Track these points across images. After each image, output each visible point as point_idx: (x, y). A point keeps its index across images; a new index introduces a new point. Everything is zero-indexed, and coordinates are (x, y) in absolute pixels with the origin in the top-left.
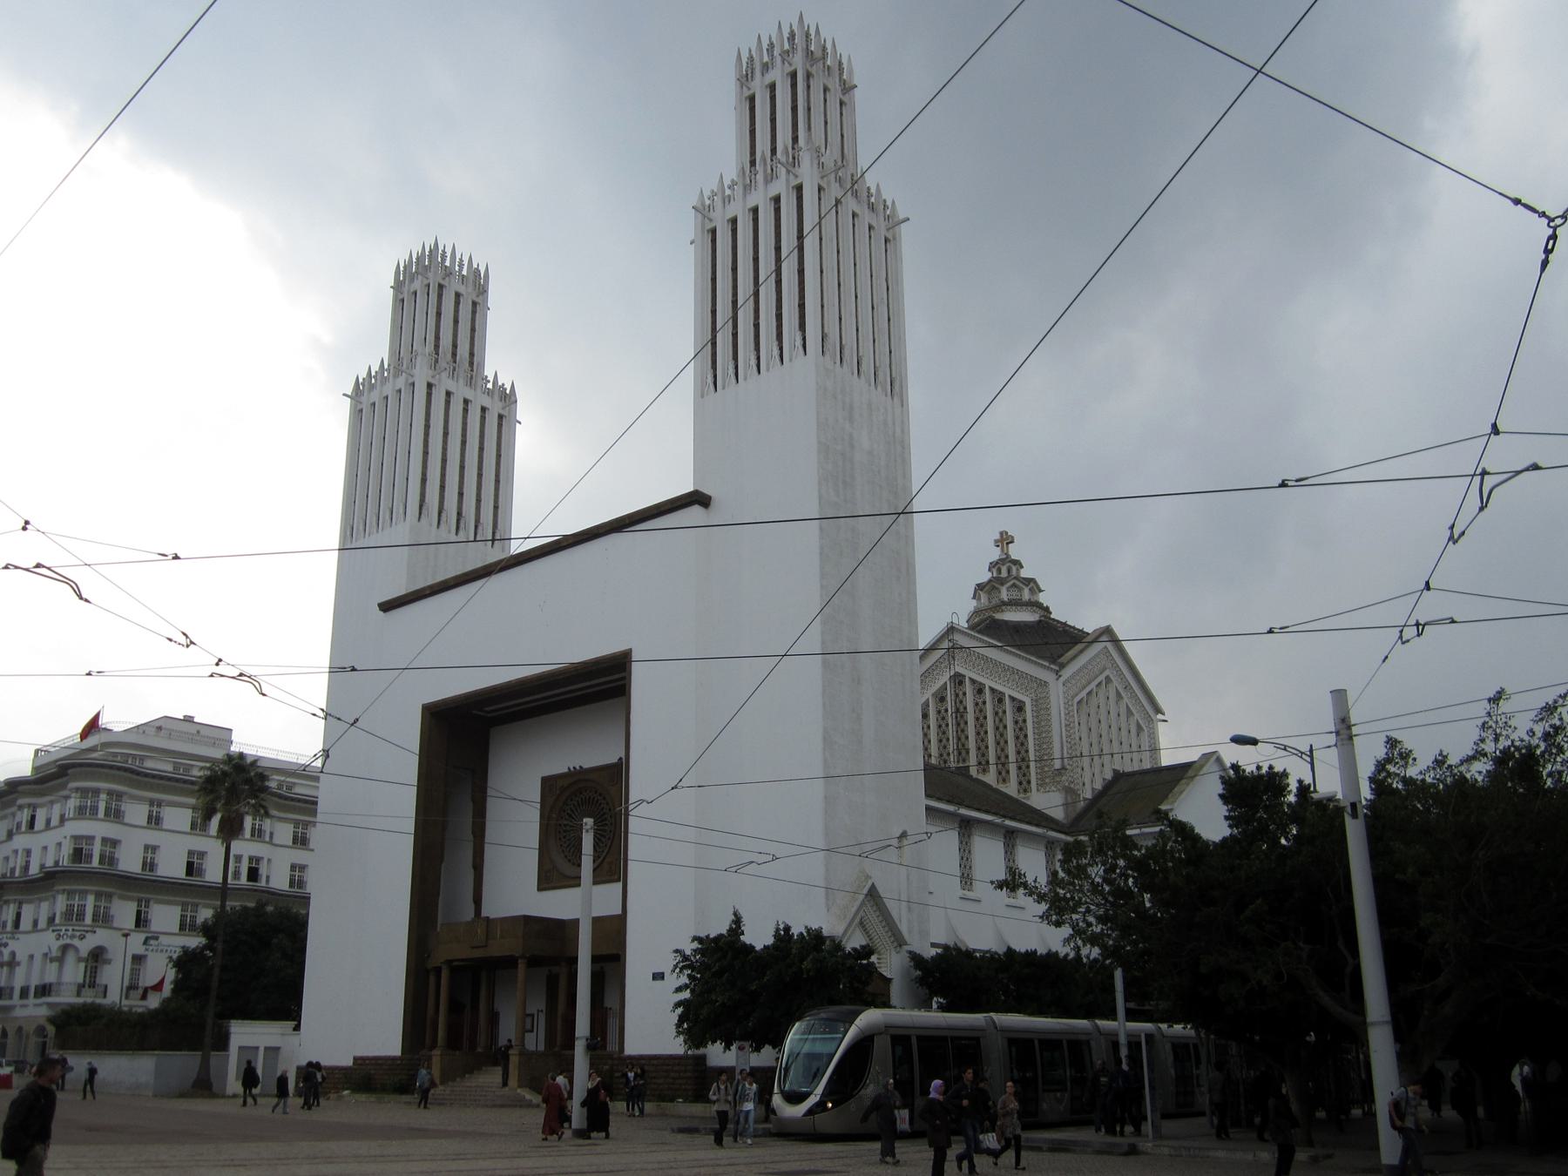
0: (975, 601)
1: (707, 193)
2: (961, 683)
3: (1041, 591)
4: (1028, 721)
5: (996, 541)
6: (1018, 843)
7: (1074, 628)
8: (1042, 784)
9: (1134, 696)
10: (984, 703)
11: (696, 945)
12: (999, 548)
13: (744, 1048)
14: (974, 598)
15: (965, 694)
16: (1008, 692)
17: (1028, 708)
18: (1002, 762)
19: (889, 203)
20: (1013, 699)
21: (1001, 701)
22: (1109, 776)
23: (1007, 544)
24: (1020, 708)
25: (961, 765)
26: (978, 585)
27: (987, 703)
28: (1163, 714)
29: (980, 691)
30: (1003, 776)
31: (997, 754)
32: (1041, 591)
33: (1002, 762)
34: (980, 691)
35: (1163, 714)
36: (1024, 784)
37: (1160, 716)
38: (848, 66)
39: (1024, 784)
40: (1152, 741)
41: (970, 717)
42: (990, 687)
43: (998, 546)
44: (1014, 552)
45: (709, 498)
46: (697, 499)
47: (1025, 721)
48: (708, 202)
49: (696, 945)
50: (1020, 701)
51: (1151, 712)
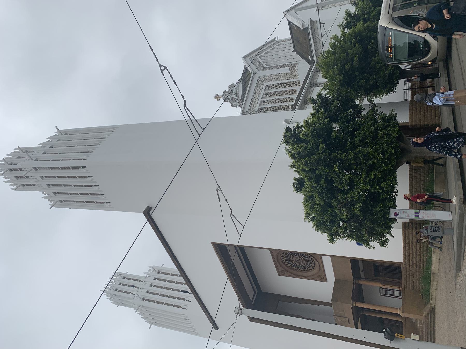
0: (237, 107)
1: (44, 196)
2: (261, 109)
3: (233, 84)
4: (295, 80)
5: (218, 100)
6: (315, 82)
7: (243, 71)
8: (296, 76)
9: (268, 48)
10: (268, 100)
11: (371, 243)
12: (220, 99)
13: (396, 213)
14: (236, 107)
15: (265, 108)
16: (263, 92)
17: (268, 84)
18: (287, 92)
19: (48, 140)
20: (265, 90)
21: (266, 94)
22: (295, 53)
23: (218, 96)
24: (269, 87)
25: (291, 108)
26: (231, 106)
27: (278, 98)
28: (275, 38)
29: (264, 102)
30: (293, 92)
31: (281, 95)
32: (233, 84)
33: (287, 92)
34: (264, 102)
35: (275, 38)
36: (297, 83)
37: (276, 39)
38: (16, 150)
39: (297, 83)
40: (281, 41)
41: (273, 105)
42: (262, 99)
43: (219, 99)
44: (221, 94)
45: (148, 207)
46: (148, 213)
47: (273, 85)
48: (47, 195)
49: (371, 243)
50: (266, 87)
51: (275, 42)
